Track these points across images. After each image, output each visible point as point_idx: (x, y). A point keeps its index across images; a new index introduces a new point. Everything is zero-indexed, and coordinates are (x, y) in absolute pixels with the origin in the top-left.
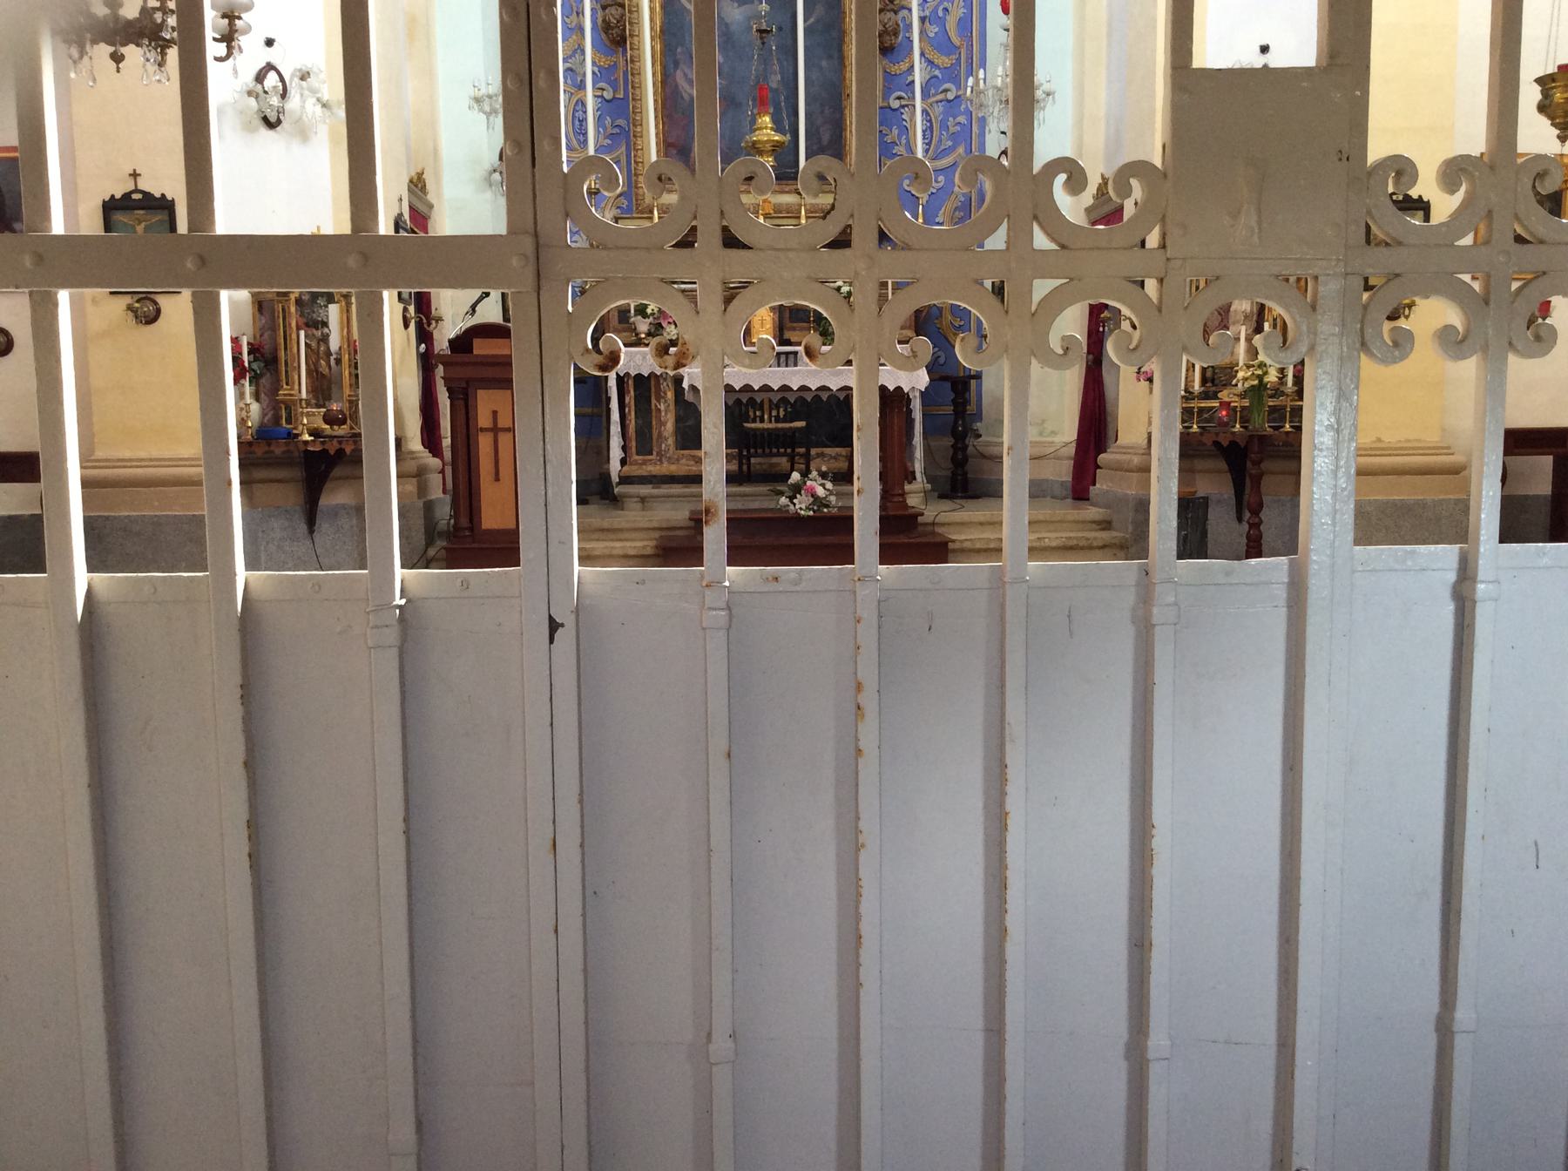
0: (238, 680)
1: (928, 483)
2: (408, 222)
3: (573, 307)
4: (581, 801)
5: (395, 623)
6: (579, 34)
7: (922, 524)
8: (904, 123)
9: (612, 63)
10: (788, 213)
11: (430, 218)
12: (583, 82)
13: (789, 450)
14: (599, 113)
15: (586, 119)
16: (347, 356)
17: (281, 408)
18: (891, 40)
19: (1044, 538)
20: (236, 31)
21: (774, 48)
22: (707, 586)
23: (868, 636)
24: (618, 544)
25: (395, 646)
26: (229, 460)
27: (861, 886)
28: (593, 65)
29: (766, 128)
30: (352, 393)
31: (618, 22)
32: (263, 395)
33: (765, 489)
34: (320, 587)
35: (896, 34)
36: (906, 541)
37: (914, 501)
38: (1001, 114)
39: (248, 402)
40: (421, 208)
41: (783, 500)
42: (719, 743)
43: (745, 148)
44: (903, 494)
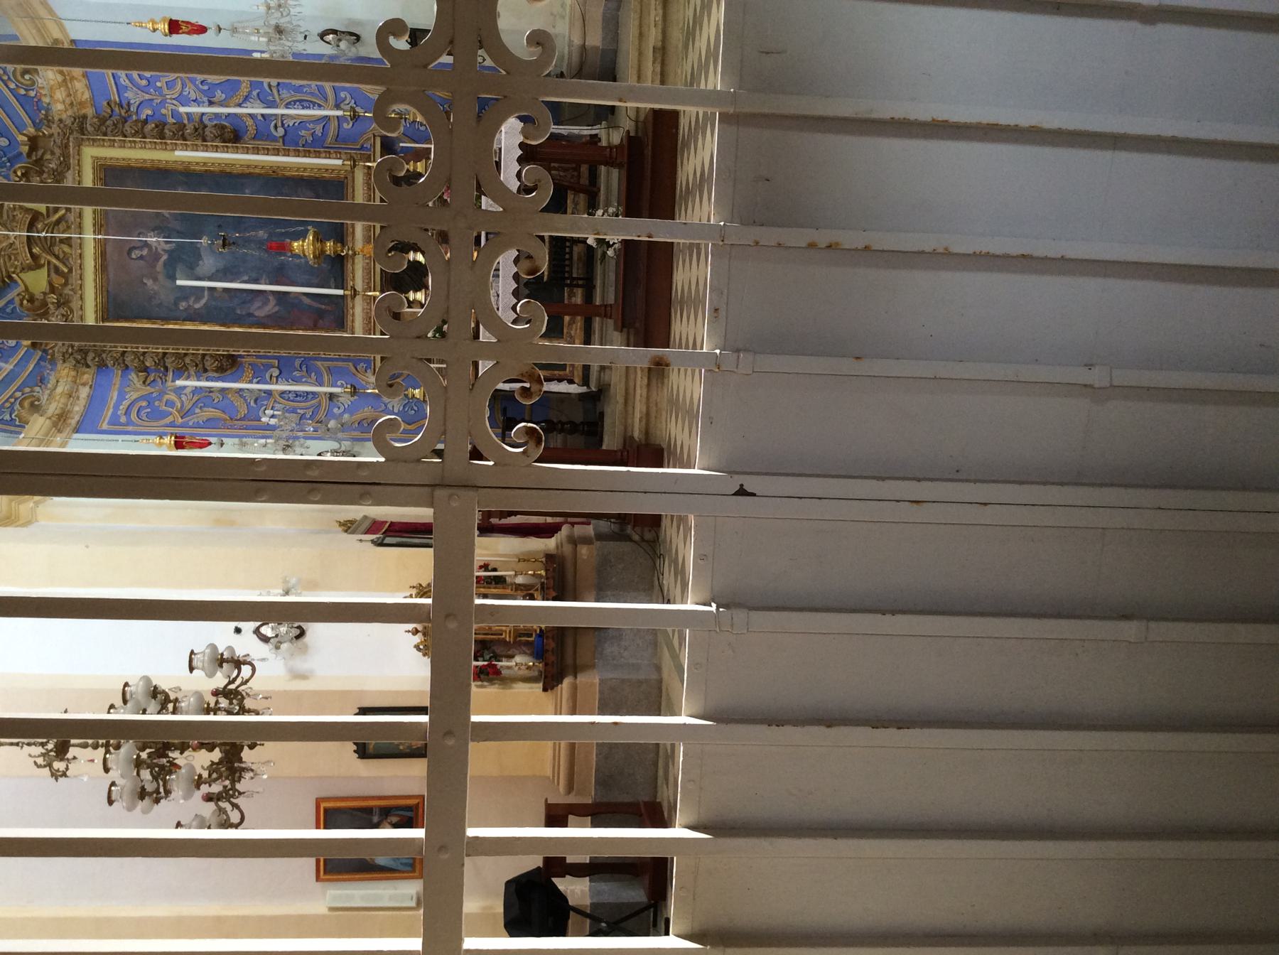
0: (765, 727)
1: (601, 124)
2: (378, 536)
3: (489, 461)
4: (883, 479)
5: (730, 612)
6: (227, 392)
7: (637, 131)
8: (296, 124)
9: (250, 367)
10: (370, 231)
11: (374, 519)
12: (266, 392)
13: (568, 244)
14: (290, 380)
15: (295, 391)
16: (482, 589)
17: (520, 640)
18: (228, 132)
19: (655, 21)
20: (232, 658)
21: (237, 235)
22: (719, 368)
23: (770, 236)
24: (638, 391)
25: (748, 613)
26: (598, 723)
27: (980, 253)
28: (252, 383)
29: (303, 246)
30: (510, 587)
31: (217, 360)
32: (509, 652)
33: (599, 267)
34: (697, 664)
35: (223, 127)
36: (650, 148)
37: (616, 138)
38: (290, 39)
39: (515, 664)
40: (366, 525)
41: (610, 253)
42: (847, 365)
43: (319, 264)
44: (610, 147)
